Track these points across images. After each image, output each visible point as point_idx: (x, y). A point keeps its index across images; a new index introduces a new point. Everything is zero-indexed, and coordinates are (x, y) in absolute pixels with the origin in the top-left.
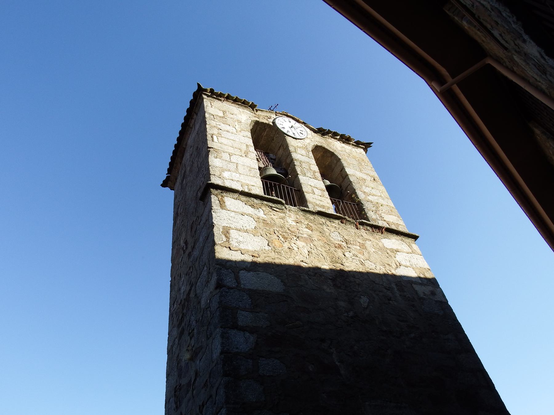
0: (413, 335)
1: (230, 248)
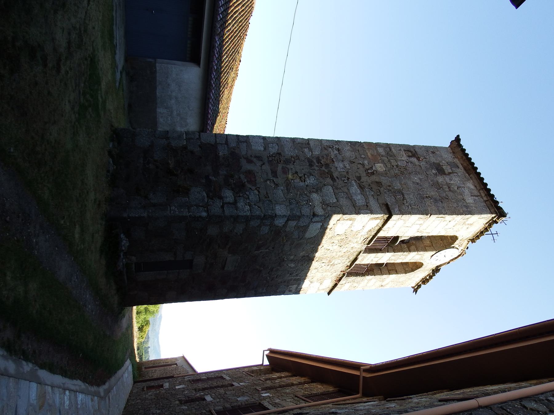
0: (268, 278)
1: (339, 220)
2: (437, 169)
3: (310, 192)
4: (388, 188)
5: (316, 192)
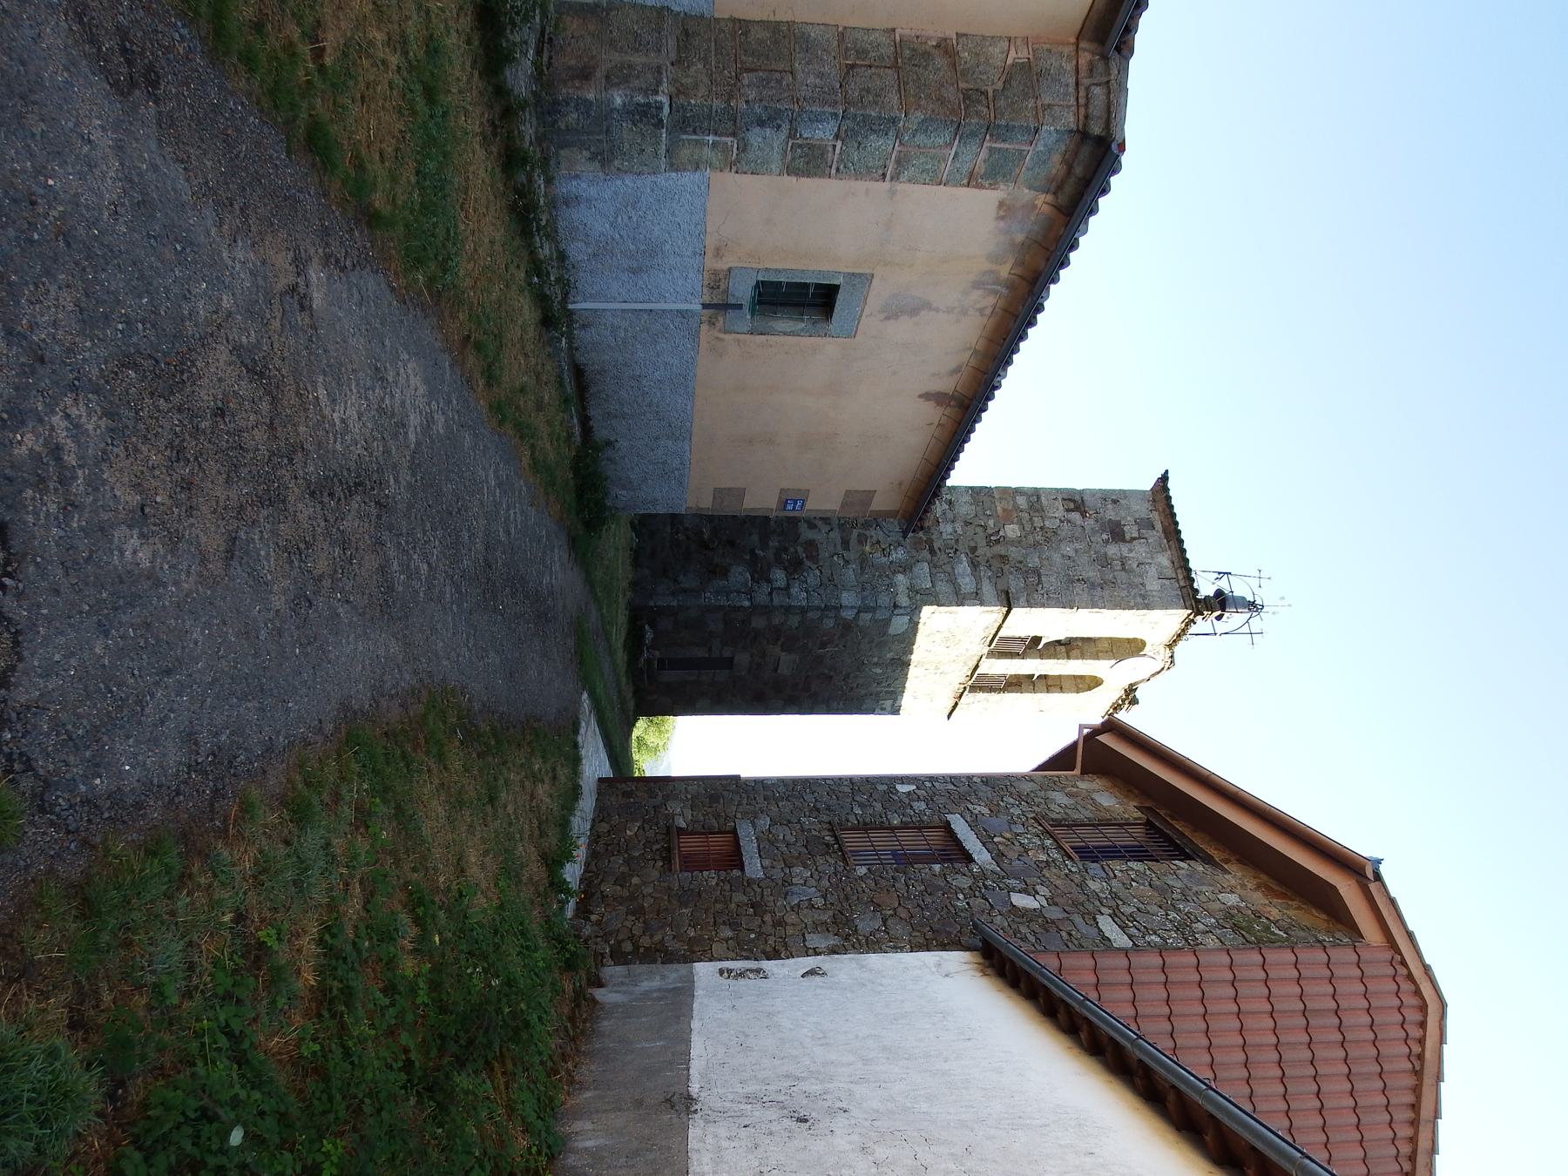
2: (1112, 532)
3: (894, 573)
4: (1018, 565)
5: (904, 572)
